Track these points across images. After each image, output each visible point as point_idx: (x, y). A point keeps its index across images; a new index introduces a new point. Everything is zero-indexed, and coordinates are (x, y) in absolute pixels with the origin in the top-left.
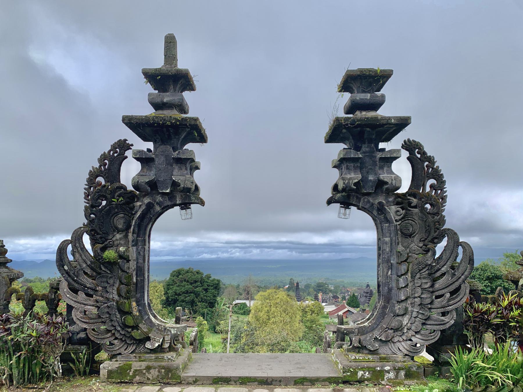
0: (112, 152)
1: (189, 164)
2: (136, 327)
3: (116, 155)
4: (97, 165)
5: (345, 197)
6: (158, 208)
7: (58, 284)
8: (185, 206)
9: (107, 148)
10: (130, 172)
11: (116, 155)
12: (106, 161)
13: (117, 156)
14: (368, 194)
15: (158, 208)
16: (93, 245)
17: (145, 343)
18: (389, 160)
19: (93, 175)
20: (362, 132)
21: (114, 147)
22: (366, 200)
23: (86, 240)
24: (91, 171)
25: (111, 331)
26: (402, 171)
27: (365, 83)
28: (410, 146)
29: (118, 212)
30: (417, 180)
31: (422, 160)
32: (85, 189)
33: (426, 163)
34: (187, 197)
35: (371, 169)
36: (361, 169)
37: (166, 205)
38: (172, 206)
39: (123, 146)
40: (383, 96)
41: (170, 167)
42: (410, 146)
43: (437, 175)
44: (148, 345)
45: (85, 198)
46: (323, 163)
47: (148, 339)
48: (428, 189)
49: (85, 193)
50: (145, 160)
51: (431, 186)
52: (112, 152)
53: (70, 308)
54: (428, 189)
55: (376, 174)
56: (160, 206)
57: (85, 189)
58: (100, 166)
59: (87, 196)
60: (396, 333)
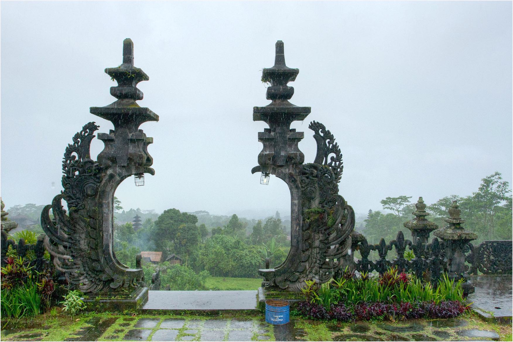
0: (83, 132)
1: (144, 142)
2: (102, 271)
3: (86, 134)
4: (72, 143)
5: (266, 165)
6: (118, 178)
7: (43, 239)
8: (139, 175)
9: (79, 129)
10: (97, 148)
11: (86, 134)
12: (79, 139)
13: (87, 135)
14: (281, 166)
15: (118, 178)
16: (69, 207)
17: (110, 283)
18: (300, 136)
19: (69, 150)
20: (279, 115)
21: (85, 128)
22: (280, 171)
23: (64, 203)
24: (67, 148)
25: (83, 274)
26: (308, 149)
27: (279, 77)
28: (316, 126)
29: (88, 180)
30: (322, 152)
31: (324, 139)
32: (63, 162)
33: (328, 140)
34: (142, 166)
35: (282, 147)
36: (275, 146)
37: (123, 175)
38: (130, 175)
39: (91, 127)
40: (292, 90)
41: (126, 146)
42: (316, 126)
43: (336, 149)
44: (112, 285)
45: (63, 169)
46: (248, 141)
47: (112, 280)
48: (329, 161)
49: (63, 165)
50: (106, 139)
51: (332, 158)
52: (83, 132)
53: (52, 257)
54: (329, 161)
55: (286, 151)
56: (120, 176)
57: (63, 162)
58: (74, 144)
59: (64, 166)
60: (302, 275)
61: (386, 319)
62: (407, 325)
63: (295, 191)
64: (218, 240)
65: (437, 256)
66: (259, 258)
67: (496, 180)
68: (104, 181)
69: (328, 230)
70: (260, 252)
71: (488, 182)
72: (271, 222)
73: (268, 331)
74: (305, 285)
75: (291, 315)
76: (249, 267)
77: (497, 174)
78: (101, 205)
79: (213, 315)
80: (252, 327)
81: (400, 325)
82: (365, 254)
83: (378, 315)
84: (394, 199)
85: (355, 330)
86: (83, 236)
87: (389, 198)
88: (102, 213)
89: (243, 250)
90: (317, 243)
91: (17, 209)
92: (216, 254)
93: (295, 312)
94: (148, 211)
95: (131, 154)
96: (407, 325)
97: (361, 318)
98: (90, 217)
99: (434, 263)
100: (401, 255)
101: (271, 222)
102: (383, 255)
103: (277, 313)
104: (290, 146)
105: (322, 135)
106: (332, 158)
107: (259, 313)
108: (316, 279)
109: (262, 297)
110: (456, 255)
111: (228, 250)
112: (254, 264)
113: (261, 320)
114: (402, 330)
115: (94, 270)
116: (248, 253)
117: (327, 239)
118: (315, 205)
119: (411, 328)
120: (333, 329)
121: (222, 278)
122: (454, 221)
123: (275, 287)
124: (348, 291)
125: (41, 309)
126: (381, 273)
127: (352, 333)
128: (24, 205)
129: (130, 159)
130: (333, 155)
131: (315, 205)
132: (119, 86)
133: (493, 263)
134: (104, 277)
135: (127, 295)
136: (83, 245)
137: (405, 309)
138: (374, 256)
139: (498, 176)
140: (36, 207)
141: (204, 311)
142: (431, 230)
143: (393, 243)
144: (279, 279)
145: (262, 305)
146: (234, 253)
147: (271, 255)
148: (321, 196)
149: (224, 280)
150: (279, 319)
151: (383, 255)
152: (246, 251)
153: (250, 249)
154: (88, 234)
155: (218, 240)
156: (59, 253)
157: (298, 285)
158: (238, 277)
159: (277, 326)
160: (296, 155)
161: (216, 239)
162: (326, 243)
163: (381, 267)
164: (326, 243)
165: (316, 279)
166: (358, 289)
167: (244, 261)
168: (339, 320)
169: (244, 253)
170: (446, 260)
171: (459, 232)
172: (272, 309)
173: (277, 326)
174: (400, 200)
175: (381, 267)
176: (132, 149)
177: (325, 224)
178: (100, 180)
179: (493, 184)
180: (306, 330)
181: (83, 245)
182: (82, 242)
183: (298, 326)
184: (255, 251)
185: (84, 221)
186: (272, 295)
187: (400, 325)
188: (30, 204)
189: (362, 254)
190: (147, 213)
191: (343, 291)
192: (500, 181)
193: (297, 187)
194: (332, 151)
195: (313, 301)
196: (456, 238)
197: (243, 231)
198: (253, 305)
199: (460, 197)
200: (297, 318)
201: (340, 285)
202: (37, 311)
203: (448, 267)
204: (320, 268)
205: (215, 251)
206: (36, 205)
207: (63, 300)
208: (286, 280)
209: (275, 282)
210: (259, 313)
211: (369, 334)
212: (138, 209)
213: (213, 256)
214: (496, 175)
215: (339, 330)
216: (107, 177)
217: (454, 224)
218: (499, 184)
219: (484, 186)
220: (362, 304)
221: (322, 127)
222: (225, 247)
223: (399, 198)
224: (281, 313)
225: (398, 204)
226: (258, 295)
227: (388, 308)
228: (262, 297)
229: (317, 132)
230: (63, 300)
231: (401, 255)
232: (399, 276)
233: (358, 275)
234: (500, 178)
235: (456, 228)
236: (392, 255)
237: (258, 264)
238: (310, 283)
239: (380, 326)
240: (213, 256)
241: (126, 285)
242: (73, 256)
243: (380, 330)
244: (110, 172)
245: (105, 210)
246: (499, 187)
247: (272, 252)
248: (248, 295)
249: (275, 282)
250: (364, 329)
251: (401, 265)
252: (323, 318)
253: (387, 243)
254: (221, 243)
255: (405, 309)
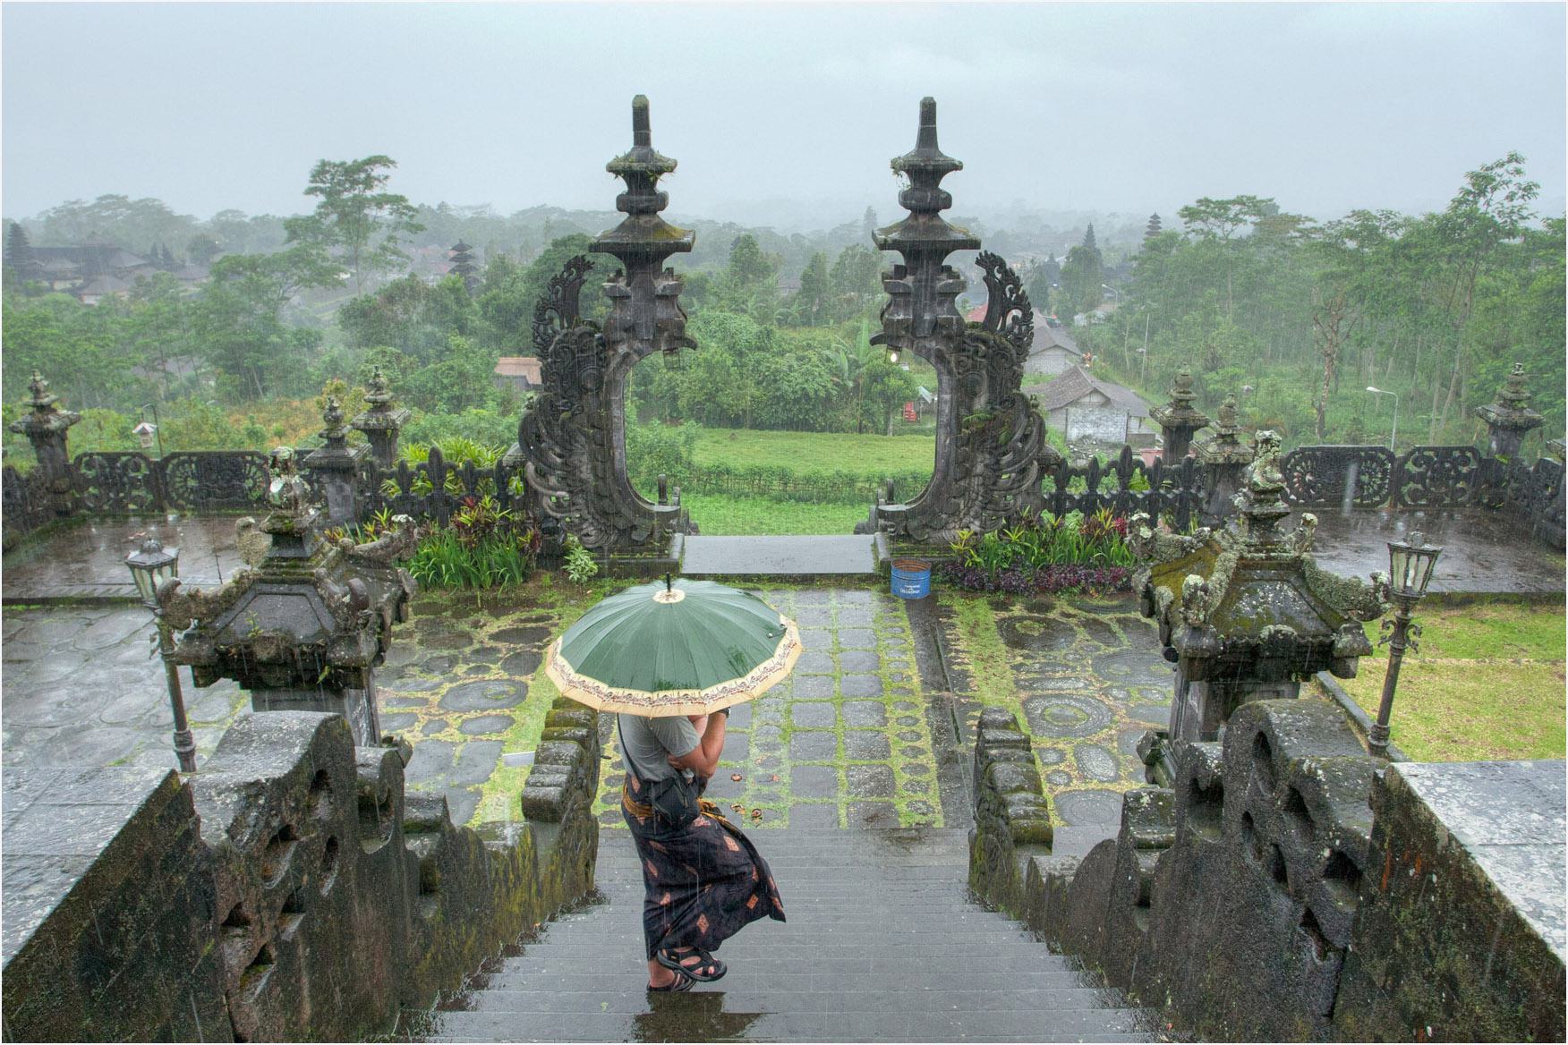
26: (973, 307)
44: (635, 536)
47: (634, 527)
48: (1009, 321)
51: (1015, 318)
54: (1009, 321)
61: (1084, 592)
62: (1115, 603)
63: (945, 378)
64: (713, 327)
65: (1187, 488)
66: (826, 377)
67: (1506, 177)
68: (613, 365)
69: (997, 450)
70: (829, 360)
71: (1482, 182)
72: (854, 256)
73: (896, 609)
74: (959, 535)
75: (933, 582)
76: (797, 401)
77: (1513, 158)
78: (607, 405)
79: (806, 581)
80: (866, 602)
81: (1105, 603)
82: (1062, 482)
83: (1071, 585)
84: (1223, 205)
85: (1030, 609)
86: (585, 458)
87: (1206, 202)
88: (610, 418)
89: (782, 354)
90: (979, 468)
91: (73, 212)
92: (710, 367)
93: (939, 577)
94: (470, 208)
95: (662, 321)
96: (1115, 603)
97: (1044, 590)
98: (593, 426)
99: (1180, 498)
100: (1125, 486)
101: (854, 256)
102: (1093, 484)
103: (911, 582)
104: (941, 304)
105: (999, 276)
106: (1015, 318)
107: (880, 579)
108: (976, 527)
109: (883, 555)
110: (1220, 488)
111: (741, 354)
112: (812, 394)
113: (886, 591)
114: (1106, 610)
115: (605, 514)
116: (795, 364)
117: (998, 462)
118: (980, 403)
119: (1120, 608)
120: (998, 606)
121: (728, 432)
122: (1223, 431)
123: (907, 536)
124: (1026, 548)
125: (523, 575)
126: (1088, 515)
127: (1026, 613)
128: (91, 201)
129: (659, 329)
130: (1016, 312)
131: (980, 403)
132: (630, 192)
133: (1310, 485)
134: (621, 524)
135: (661, 551)
136: (586, 473)
137: (1115, 578)
138: (1078, 488)
139: (1514, 165)
140: (130, 206)
141: (790, 576)
142: (1197, 428)
143: (1113, 464)
144: (913, 524)
145: (885, 566)
146: (758, 362)
147: (859, 367)
148: (992, 389)
149: (733, 438)
150: (913, 590)
151: (1093, 484)
152: (790, 359)
153: (800, 353)
154: (593, 457)
155: (713, 327)
156: (551, 488)
157: (945, 534)
158: (772, 427)
159: (910, 602)
160: (949, 321)
161: (707, 323)
162: (996, 469)
163: (1088, 505)
164: (996, 469)
165: (976, 527)
166: (1044, 544)
167: (785, 386)
168: (1008, 592)
169: (782, 363)
170: (1202, 494)
171: (1228, 449)
172: (902, 575)
173: (910, 602)
174: (1238, 207)
175: (1088, 505)
176: (662, 312)
177: (996, 438)
178: (604, 362)
179: (1494, 189)
180: (956, 608)
181: (586, 473)
182: (584, 468)
183: (943, 601)
184: (815, 359)
185: (586, 435)
186: (901, 549)
187: (1105, 603)
188: (111, 197)
189: (1057, 481)
190: (469, 214)
191: (1017, 549)
192: (1516, 179)
193: (950, 373)
194: (1017, 305)
195: (968, 563)
196: (1221, 460)
197: (770, 281)
198: (868, 566)
199: (1404, 215)
200: (942, 587)
201: (1014, 537)
202: (520, 580)
203: (1205, 506)
204: (984, 508)
205: (705, 360)
206: (131, 199)
207: (568, 562)
208: (926, 526)
209: (906, 529)
210: (880, 579)
211: (1051, 615)
212: (442, 206)
213: (702, 373)
214: (1509, 161)
215: (1007, 609)
216: (618, 359)
217: (1223, 436)
218: (1512, 188)
219: (1469, 193)
220: (1047, 568)
221: (1001, 263)
222: (731, 347)
223: (1234, 202)
224: (917, 581)
225: (1228, 219)
226: (875, 545)
227: (1087, 576)
228: (883, 555)
229: (990, 273)
230: (568, 562)
231: (1125, 486)
232: (1114, 524)
233: (1048, 516)
234: (1518, 172)
235: (1225, 442)
236: (1109, 485)
237: (822, 394)
238: (965, 534)
239: (1071, 604)
240: (702, 373)
241: (657, 535)
242: (570, 492)
243: (1072, 611)
244: (622, 349)
245: (616, 412)
246: (1511, 197)
247: (863, 360)
248: (859, 552)
249: (906, 529)
250: (1048, 607)
251: (1124, 503)
252: (983, 588)
253: (1102, 466)
254: (719, 335)
255: (1115, 578)
